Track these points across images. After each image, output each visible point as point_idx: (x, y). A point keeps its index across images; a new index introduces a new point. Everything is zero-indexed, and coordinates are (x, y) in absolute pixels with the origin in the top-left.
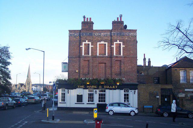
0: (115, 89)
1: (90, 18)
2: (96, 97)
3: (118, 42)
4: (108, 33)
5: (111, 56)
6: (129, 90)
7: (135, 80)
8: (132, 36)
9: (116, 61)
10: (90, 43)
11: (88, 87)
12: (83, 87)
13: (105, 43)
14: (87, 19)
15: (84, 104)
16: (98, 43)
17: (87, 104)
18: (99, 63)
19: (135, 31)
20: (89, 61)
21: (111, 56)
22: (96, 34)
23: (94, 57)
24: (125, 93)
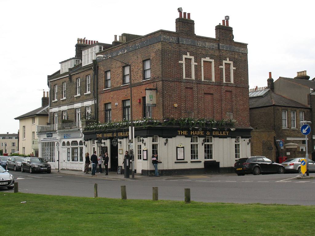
0: (225, 137)
1: (189, 14)
2: (201, 150)
3: (228, 61)
4: (214, 44)
5: (219, 83)
6: (158, 137)
7: (247, 123)
8: (242, 53)
9: (226, 91)
10: (193, 58)
11: (192, 134)
12: (185, 132)
13: (211, 60)
14: (185, 13)
15: (187, 162)
16: (203, 59)
17: (175, 162)
18: (205, 93)
19: (244, 46)
20: (192, 88)
21: (219, 83)
22: (200, 44)
23: (198, 81)
24: (193, 143)
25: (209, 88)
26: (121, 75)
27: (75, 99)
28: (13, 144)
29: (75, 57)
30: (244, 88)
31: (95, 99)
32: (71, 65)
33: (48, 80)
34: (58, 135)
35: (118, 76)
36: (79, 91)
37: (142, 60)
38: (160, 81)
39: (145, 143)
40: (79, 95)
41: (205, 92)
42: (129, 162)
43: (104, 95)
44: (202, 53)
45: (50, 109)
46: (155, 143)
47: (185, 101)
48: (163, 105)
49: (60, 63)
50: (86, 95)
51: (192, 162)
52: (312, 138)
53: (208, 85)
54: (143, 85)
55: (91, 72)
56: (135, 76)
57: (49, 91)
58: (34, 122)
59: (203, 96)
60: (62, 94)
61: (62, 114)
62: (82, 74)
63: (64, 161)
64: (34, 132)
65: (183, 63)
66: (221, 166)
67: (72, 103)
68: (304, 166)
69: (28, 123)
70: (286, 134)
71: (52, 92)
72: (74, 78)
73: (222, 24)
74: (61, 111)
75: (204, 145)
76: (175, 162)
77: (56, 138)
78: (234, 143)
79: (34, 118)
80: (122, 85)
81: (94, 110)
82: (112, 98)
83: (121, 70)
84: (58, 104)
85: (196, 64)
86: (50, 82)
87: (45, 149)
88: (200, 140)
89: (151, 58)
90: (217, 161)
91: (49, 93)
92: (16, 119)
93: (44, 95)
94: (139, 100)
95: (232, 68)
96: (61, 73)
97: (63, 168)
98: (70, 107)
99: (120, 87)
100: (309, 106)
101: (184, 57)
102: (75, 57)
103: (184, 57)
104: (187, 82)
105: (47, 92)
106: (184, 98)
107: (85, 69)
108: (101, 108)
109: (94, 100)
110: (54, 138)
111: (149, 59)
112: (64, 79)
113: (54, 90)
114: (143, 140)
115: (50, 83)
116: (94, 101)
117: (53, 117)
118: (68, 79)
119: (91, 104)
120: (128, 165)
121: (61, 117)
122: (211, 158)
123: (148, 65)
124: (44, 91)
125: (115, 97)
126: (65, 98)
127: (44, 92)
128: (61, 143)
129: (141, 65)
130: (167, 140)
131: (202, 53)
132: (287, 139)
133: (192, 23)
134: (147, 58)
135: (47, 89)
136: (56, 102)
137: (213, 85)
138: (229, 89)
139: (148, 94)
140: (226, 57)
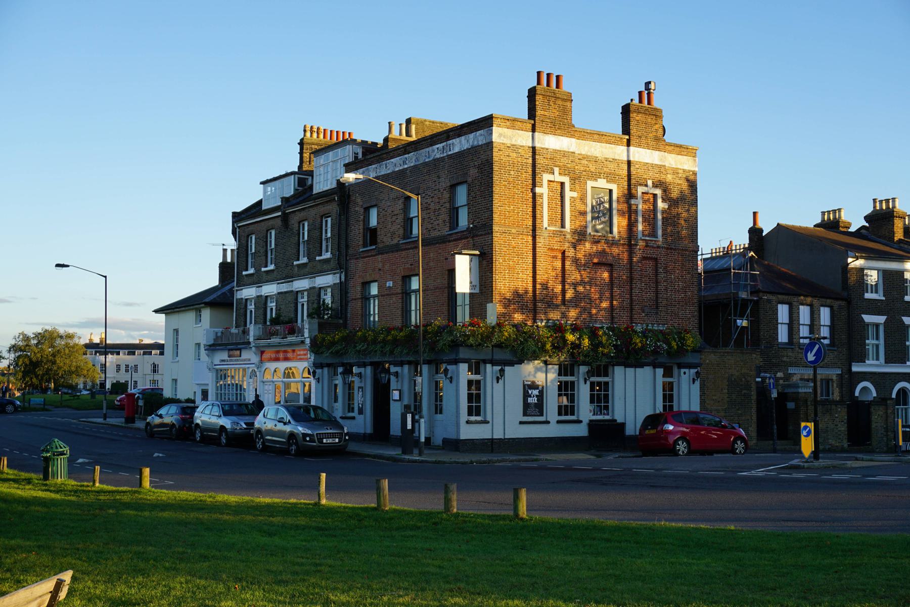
15: (548, 422)
16: (590, 184)
17: (521, 423)
26: (401, 218)
27: (296, 269)
28: (155, 369)
29: (297, 170)
31: (342, 272)
32: (289, 188)
34: (255, 353)
36: (304, 251)
37: (449, 184)
39: (451, 378)
40: (304, 260)
42: (414, 421)
43: (361, 264)
44: (588, 169)
45: (237, 290)
49: (261, 183)
50: (320, 261)
51: (559, 422)
54: (450, 241)
55: (334, 208)
56: (432, 221)
57: (235, 247)
58: (199, 319)
60: (267, 257)
61: (266, 303)
62: (313, 212)
64: (198, 345)
67: (289, 277)
68: (808, 438)
69: (187, 319)
70: (788, 360)
71: (242, 250)
72: (294, 220)
74: (261, 296)
75: (588, 383)
76: (521, 423)
77: (249, 360)
79: (200, 311)
80: (404, 241)
81: (338, 297)
82: (380, 270)
83: (402, 206)
84: (258, 280)
86: (239, 227)
89: (470, 180)
90: (618, 421)
91: (236, 253)
92: (156, 311)
94: (447, 272)
96: (265, 207)
98: (284, 288)
99: (397, 245)
102: (297, 170)
105: (232, 251)
106: (544, 275)
107: (319, 201)
108: (355, 291)
109: (338, 273)
110: (245, 360)
112: (271, 222)
113: (247, 244)
114: (446, 371)
115: (238, 230)
116: (338, 275)
117: (244, 310)
118: (279, 222)
119: (331, 283)
120: (409, 427)
121: (261, 311)
124: (225, 247)
125: (387, 267)
126: (271, 267)
127: (225, 251)
128: (260, 372)
129: (446, 195)
130: (502, 371)
131: (588, 169)
132: (789, 372)
135: (232, 244)
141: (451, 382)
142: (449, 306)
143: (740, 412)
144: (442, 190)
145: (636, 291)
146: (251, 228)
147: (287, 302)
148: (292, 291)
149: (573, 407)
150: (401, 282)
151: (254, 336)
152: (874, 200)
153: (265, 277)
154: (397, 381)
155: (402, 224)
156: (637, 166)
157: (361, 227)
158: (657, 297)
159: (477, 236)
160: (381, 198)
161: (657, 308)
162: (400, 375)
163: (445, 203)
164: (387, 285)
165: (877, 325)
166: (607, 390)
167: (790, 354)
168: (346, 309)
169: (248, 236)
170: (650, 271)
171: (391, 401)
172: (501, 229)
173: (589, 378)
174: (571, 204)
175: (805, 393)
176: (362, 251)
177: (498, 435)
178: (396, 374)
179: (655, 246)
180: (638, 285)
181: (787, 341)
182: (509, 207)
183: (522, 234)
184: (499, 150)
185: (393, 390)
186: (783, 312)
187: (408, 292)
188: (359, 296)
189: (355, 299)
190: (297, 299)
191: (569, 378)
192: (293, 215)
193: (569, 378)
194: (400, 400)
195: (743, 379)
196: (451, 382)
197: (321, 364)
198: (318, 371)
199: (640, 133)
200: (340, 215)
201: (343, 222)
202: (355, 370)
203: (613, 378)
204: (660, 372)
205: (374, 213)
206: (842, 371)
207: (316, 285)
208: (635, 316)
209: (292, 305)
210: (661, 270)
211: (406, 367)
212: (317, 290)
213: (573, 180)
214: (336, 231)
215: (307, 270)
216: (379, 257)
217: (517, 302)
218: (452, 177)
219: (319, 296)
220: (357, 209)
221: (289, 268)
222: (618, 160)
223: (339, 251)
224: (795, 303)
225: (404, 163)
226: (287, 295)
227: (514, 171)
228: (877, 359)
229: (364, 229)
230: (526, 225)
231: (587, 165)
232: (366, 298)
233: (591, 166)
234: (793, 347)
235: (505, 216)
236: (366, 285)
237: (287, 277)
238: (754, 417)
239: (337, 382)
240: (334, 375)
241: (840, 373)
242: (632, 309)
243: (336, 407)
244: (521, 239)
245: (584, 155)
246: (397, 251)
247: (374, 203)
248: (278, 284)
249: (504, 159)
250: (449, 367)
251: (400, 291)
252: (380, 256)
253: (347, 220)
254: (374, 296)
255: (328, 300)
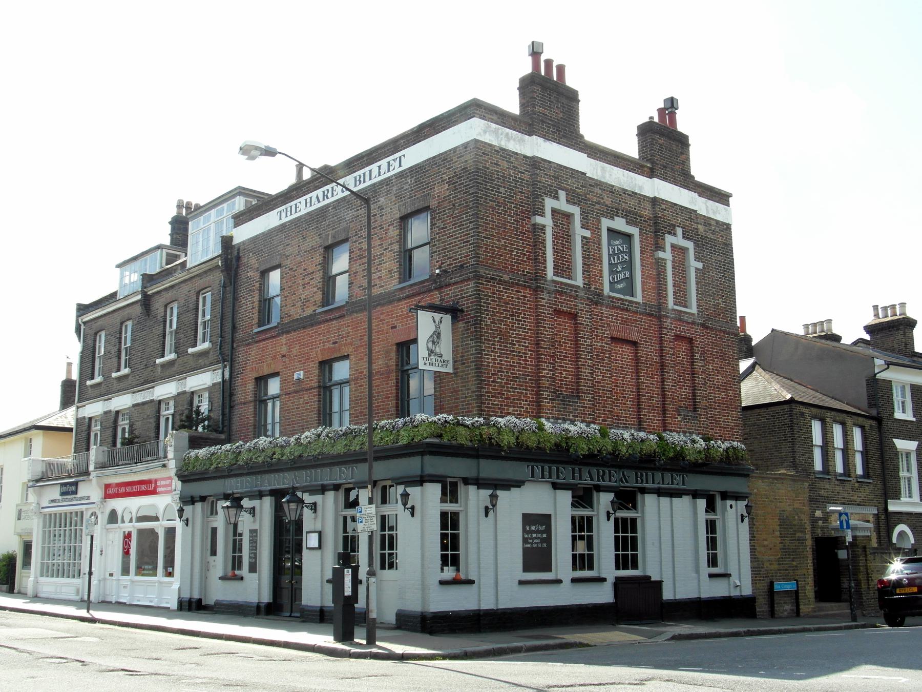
1: (561, 69)
3: (679, 240)
5: (656, 312)
9: (677, 337)
10: (575, 210)
15: (559, 582)
16: (606, 223)
17: (521, 583)
18: (613, 339)
25: (625, 322)
26: (318, 276)
27: (159, 369)
30: (724, 332)
31: (225, 366)
33: (78, 317)
35: (307, 280)
36: (171, 344)
37: (398, 216)
38: (469, 279)
40: (170, 356)
41: (615, 334)
43: (254, 351)
44: (602, 201)
46: (450, 507)
47: (553, 358)
48: (479, 367)
51: (574, 581)
52: (886, 509)
53: (623, 310)
59: (607, 347)
60: (119, 358)
63: (111, 575)
65: (544, 226)
66: (667, 594)
67: (150, 381)
71: (88, 357)
72: (157, 305)
73: (656, 120)
74: (110, 411)
77: (88, 498)
78: (702, 517)
81: (218, 402)
82: (284, 356)
85: (587, 234)
86: (85, 323)
87: (55, 536)
88: (605, 500)
93: (69, 371)
95: (694, 265)
97: (108, 599)
98: (141, 397)
99: (314, 315)
100: (874, 412)
101: (549, 204)
103: (549, 204)
104: (561, 291)
106: (549, 349)
108: (245, 391)
110: (82, 498)
111: (427, 209)
112: (128, 311)
114: (405, 496)
115: (82, 327)
116: (220, 371)
117: (86, 432)
118: (138, 309)
120: (348, 592)
122: (635, 566)
123: (419, 230)
124: (69, 361)
126: (125, 371)
130: (493, 497)
133: (572, 97)
134: (418, 205)
136: (99, 384)
137: (636, 313)
138: (686, 330)
139: (426, 323)
140: (674, 226)
141: (413, 515)
142: (397, 400)
143: (794, 563)
144: (385, 226)
145: (669, 384)
146: (100, 322)
147: (145, 416)
148: (152, 401)
149: (591, 557)
150: (317, 371)
151: (96, 463)
152: (876, 308)
153: (116, 386)
154: (315, 518)
155: (320, 285)
156: (663, 206)
157: (256, 299)
158: (694, 395)
159: (447, 285)
160: (287, 254)
161: (695, 410)
162: (319, 508)
163: (392, 244)
164: (296, 377)
165: (908, 454)
166: (634, 530)
167: (827, 486)
168: (230, 419)
169: (96, 334)
170: (683, 356)
171: (304, 551)
172: (488, 272)
173: (615, 511)
174: (582, 247)
175: (863, 536)
176: (257, 333)
177: (487, 604)
178: (314, 507)
179: (690, 320)
180: (671, 375)
181: (821, 470)
182: (499, 241)
183: (517, 284)
184: (483, 153)
185: (307, 532)
186: (816, 428)
187: (328, 384)
188: (250, 397)
189: (245, 403)
190: (159, 411)
191: (585, 512)
192: (157, 297)
193: (585, 512)
194: (320, 547)
195: (796, 518)
196: (413, 515)
197: (192, 498)
198: (188, 509)
199: (664, 162)
200: (224, 287)
201: (230, 296)
202: (246, 503)
203: (643, 512)
204: (702, 503)
205: (275, 277)
206: (878, 510)
207: (187, 389)
208: (670, 420)
209: (152, 420)
210: (697, 356)
211: (330, 495)
212: (188, 395)
213: (585, 215)
214: (218, 309)
215: (174, 369)
216: (283, 339)
217: (512, 388)
218: (405, 204)
219: (191, 403)
220: (249, 274)
221: (150, 369)
222: (640, 195)
223: (221, 336)
224: (828, 420)
225: (325, 196)
226: (146, 406)
227: (504, 187)
228: (910, 496)
229: (260, 301)
230: (523, 271)
231: (601, 195)
232: (261, 401)
233: (606, 197)
234: (829, 477)
235: (493, 254)
236: (261, 381)
237: (147, 382)
238: (811, 571)
239: (215, 525)
240: (212, 514)
241: (876, 512)
242: (664, 410)
243: (212, 563)
244: (516, 291)
245: (597, 180)
246: (312, 325)
247: (276, 262)
248: (134, 393)
249: (491, 168)
250: (409, 490)
251: (316, 385)
252: (285, 336)
253: (235, 291)
254: (274, 398)
255: (204, 408)
